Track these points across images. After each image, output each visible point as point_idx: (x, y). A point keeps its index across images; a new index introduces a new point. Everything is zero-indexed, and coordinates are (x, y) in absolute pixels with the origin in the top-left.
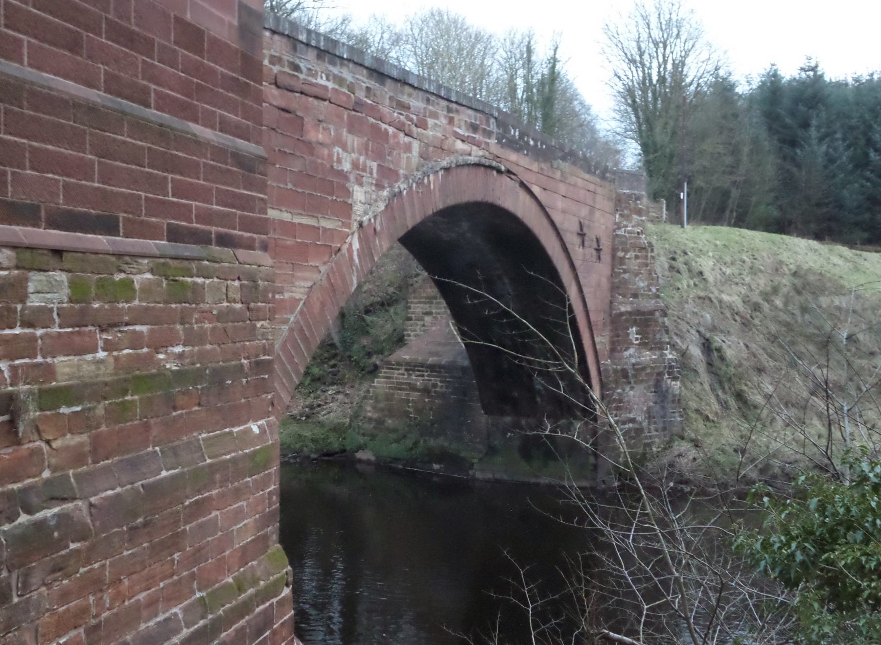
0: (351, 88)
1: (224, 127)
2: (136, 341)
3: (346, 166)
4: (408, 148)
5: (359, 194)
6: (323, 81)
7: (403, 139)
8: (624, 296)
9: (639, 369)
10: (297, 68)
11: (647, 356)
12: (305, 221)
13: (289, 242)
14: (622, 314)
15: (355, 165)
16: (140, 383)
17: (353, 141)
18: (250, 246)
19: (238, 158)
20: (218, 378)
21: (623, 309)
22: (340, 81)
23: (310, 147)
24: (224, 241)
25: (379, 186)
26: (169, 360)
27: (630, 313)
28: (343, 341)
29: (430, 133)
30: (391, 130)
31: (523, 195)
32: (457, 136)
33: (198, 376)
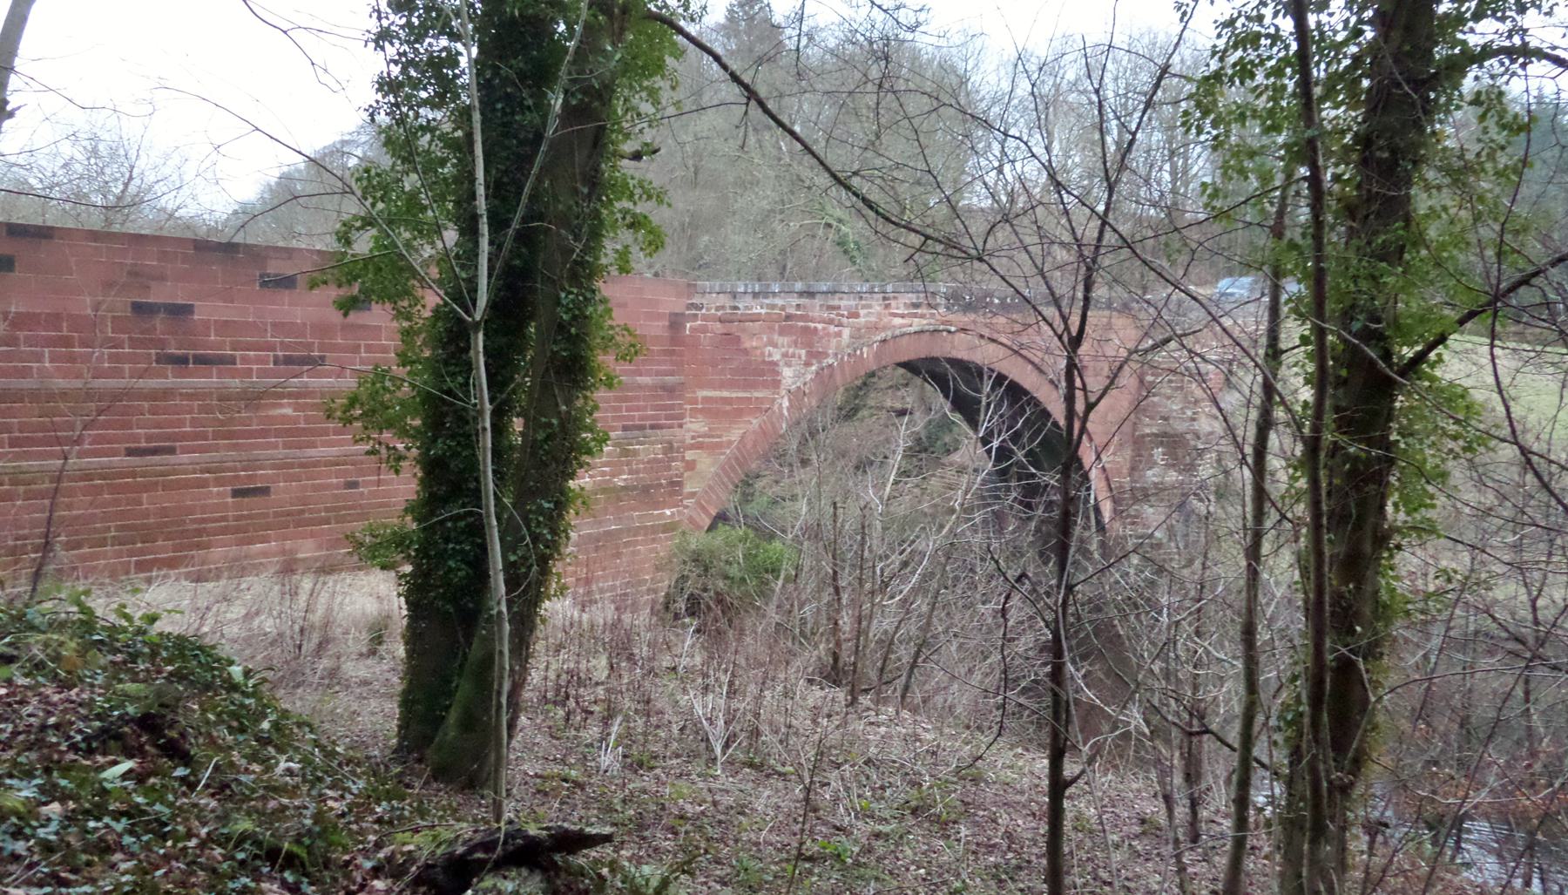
0: (783, 308)
1: (658, 373)
2: (603, 474)
3: (777, 357)
4: (839, 334)
5: (787, 373)
6: (759, 310)
7: (833, 329)
8: (1152, 418)
9: (1160, 489)
10: (736, 308)
11: (1172, 476)
12: (741, 395)
13: (728, 408)
14: (1143, 436)
15: (785, 355)
16: (604, 491)
17: (783, 340)
18: (671, 427)
19: (664, 388)
20: (646, 490)
21: (1148, 431)
22: (773, 307)
23: (746, 352)
24: (653, 427)
25: (808, 364)
26: (619, 481)
27: (1156, 435)
28: (929, 438)
29: (862, 320)
30: (820, 326)
31: (992, 346)
32: (895, 315)
33: (635, 488)
